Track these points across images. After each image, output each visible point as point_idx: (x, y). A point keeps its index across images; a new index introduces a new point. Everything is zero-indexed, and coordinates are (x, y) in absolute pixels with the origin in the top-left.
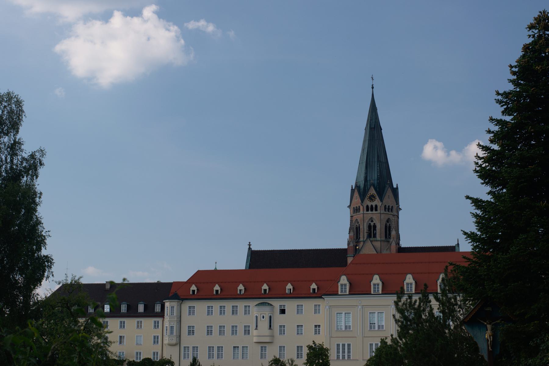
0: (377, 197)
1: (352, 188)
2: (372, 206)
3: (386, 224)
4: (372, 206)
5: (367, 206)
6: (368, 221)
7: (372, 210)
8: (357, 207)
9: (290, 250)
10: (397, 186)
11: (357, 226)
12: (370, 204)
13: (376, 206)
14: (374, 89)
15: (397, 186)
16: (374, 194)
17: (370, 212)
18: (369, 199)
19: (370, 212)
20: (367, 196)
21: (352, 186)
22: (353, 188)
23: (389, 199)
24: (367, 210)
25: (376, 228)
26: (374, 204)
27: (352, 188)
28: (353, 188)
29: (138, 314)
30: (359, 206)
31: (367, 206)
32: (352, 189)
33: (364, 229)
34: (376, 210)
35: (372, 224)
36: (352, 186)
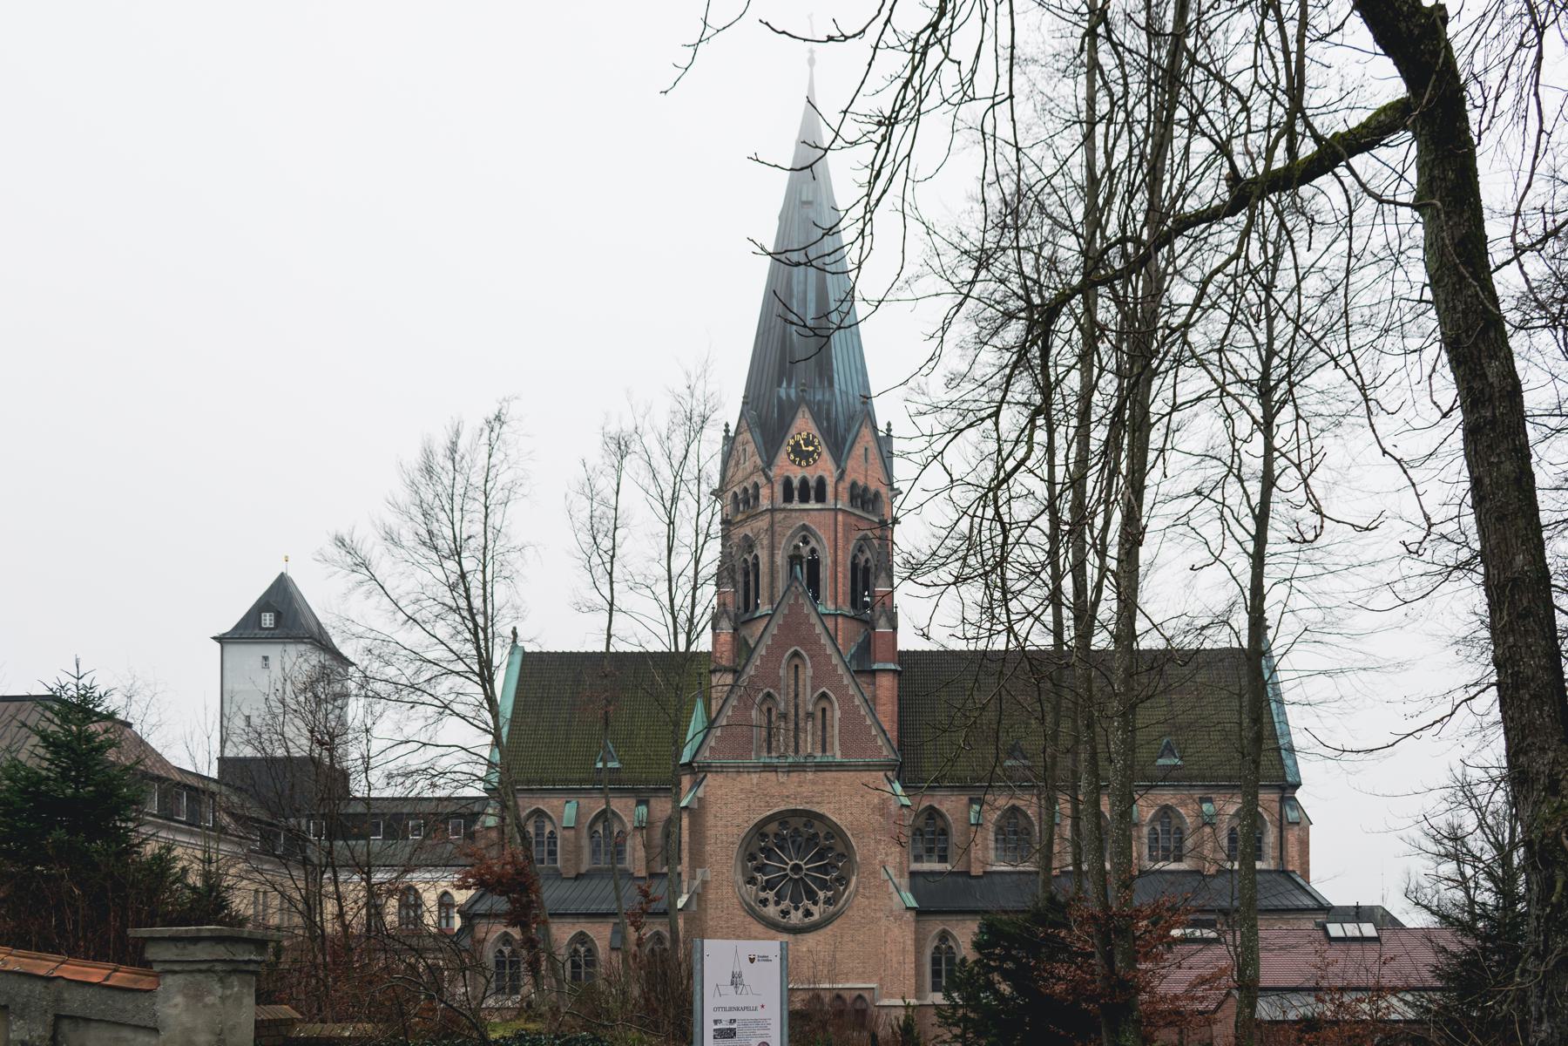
0: (823, 449)
1: (727, 431)
2: (804, 482)
3: (855, 557)
4: (804, 482)
5: (788, 483)
6: (793, 536)
7: (804, 498)
8: (746, 490)
9: (915, 652)
10: (889, 430)
11: (745, 560)
12: (797, 474)
13: (821, 482)
14: (815, 68)
15: (889, 430)
16: (814, 437)
17: (796, 505)
18: (792, 457)
19: (796, 505)
20: (786, 443)
21: (727, 425)
22: (732, 434)
23: (860, 470)
24: (788, 497)
25: (1375, 37)
26: (812, 474)
27: (727, 431)
28: (732, 434)
29: (743, 649)
30: (756, 486)
31: (788, 483)
32: (726, 437)
33: (772, 560)
34: (821, 497)
35: (805, 551)
36: (727, 425)
